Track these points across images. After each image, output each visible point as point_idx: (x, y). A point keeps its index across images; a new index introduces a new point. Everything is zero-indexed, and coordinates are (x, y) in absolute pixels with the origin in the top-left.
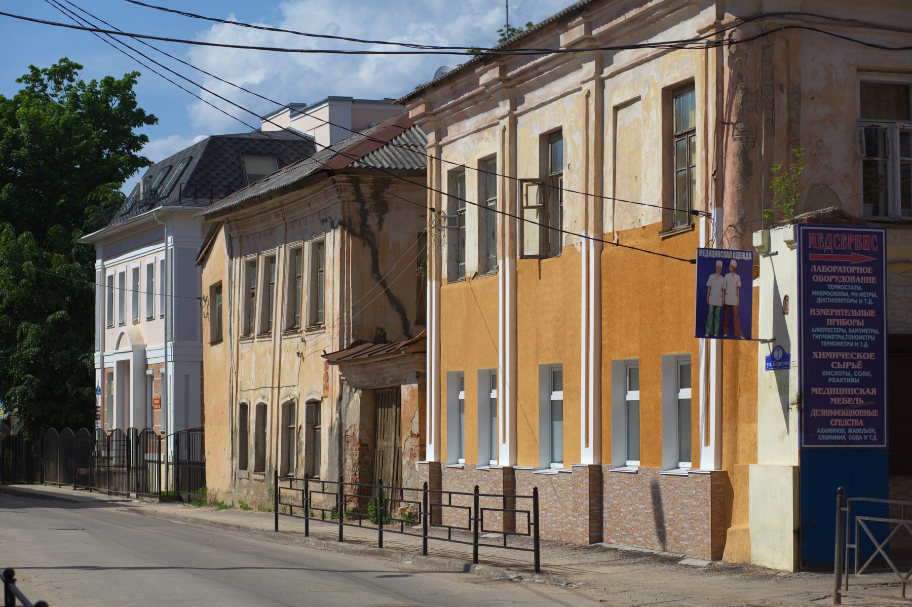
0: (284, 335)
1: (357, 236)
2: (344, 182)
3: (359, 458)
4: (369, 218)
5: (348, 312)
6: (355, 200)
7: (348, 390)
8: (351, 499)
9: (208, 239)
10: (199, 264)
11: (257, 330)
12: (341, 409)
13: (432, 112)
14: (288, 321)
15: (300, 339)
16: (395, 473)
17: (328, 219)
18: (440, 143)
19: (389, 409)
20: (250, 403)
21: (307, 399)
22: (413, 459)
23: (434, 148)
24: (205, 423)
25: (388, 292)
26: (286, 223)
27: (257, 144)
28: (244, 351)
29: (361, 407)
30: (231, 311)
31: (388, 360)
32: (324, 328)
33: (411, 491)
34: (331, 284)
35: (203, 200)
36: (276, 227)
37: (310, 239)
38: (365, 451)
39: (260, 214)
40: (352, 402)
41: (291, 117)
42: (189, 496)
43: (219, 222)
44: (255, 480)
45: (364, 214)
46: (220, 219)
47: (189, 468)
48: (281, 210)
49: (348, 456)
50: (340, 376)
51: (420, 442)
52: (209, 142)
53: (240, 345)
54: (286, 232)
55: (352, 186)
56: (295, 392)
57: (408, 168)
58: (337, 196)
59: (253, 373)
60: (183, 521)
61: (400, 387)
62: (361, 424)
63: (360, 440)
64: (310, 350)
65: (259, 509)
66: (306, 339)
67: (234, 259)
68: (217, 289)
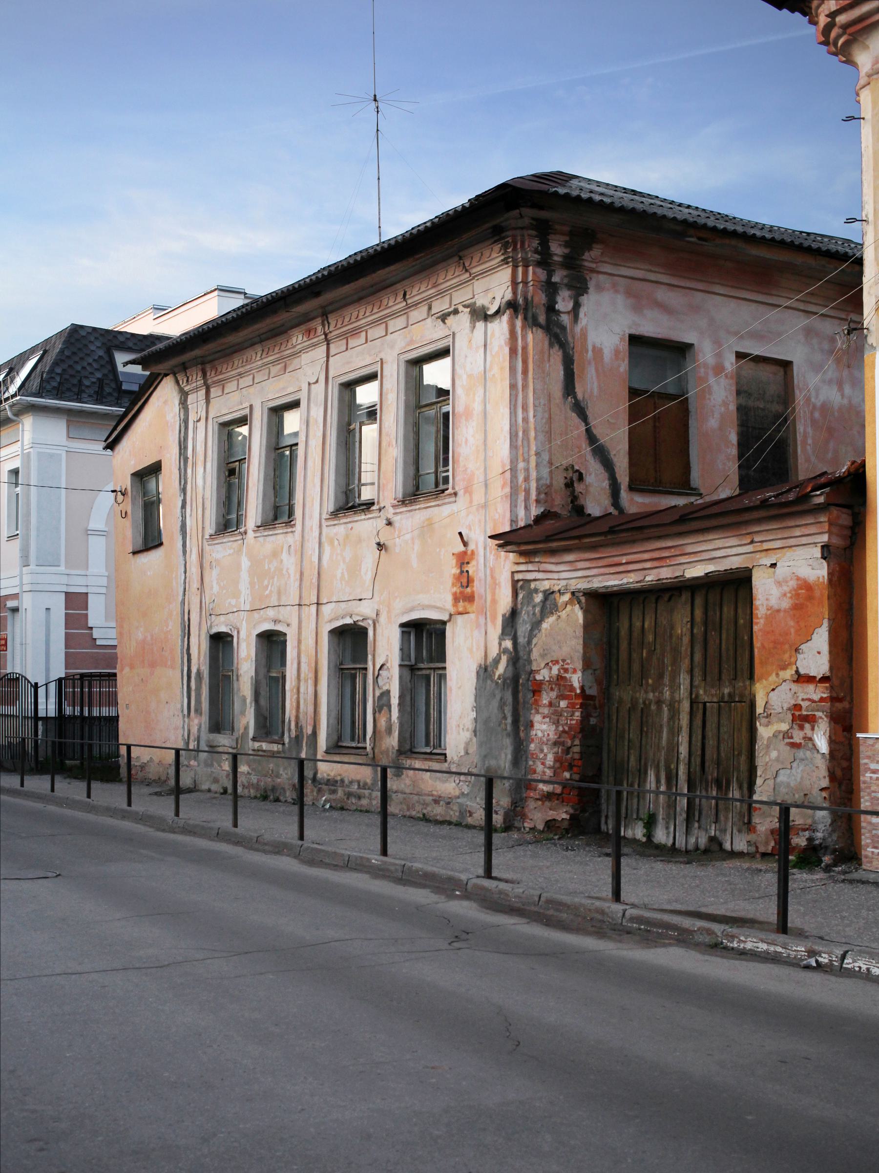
1: (541, 326)
3: (582, 721)
4: (559, 299)
15: (381, 523)
17: (461, 308)
20: (238, 632)
21: (405, 619)
22: (801, 728)
25: (588, 431)
45: (551, 289)
47: (82, 745)
49: (537, 718)
54: (328, 361)
55: (536, 236)
56: (363, 611)
63: (582, 688)
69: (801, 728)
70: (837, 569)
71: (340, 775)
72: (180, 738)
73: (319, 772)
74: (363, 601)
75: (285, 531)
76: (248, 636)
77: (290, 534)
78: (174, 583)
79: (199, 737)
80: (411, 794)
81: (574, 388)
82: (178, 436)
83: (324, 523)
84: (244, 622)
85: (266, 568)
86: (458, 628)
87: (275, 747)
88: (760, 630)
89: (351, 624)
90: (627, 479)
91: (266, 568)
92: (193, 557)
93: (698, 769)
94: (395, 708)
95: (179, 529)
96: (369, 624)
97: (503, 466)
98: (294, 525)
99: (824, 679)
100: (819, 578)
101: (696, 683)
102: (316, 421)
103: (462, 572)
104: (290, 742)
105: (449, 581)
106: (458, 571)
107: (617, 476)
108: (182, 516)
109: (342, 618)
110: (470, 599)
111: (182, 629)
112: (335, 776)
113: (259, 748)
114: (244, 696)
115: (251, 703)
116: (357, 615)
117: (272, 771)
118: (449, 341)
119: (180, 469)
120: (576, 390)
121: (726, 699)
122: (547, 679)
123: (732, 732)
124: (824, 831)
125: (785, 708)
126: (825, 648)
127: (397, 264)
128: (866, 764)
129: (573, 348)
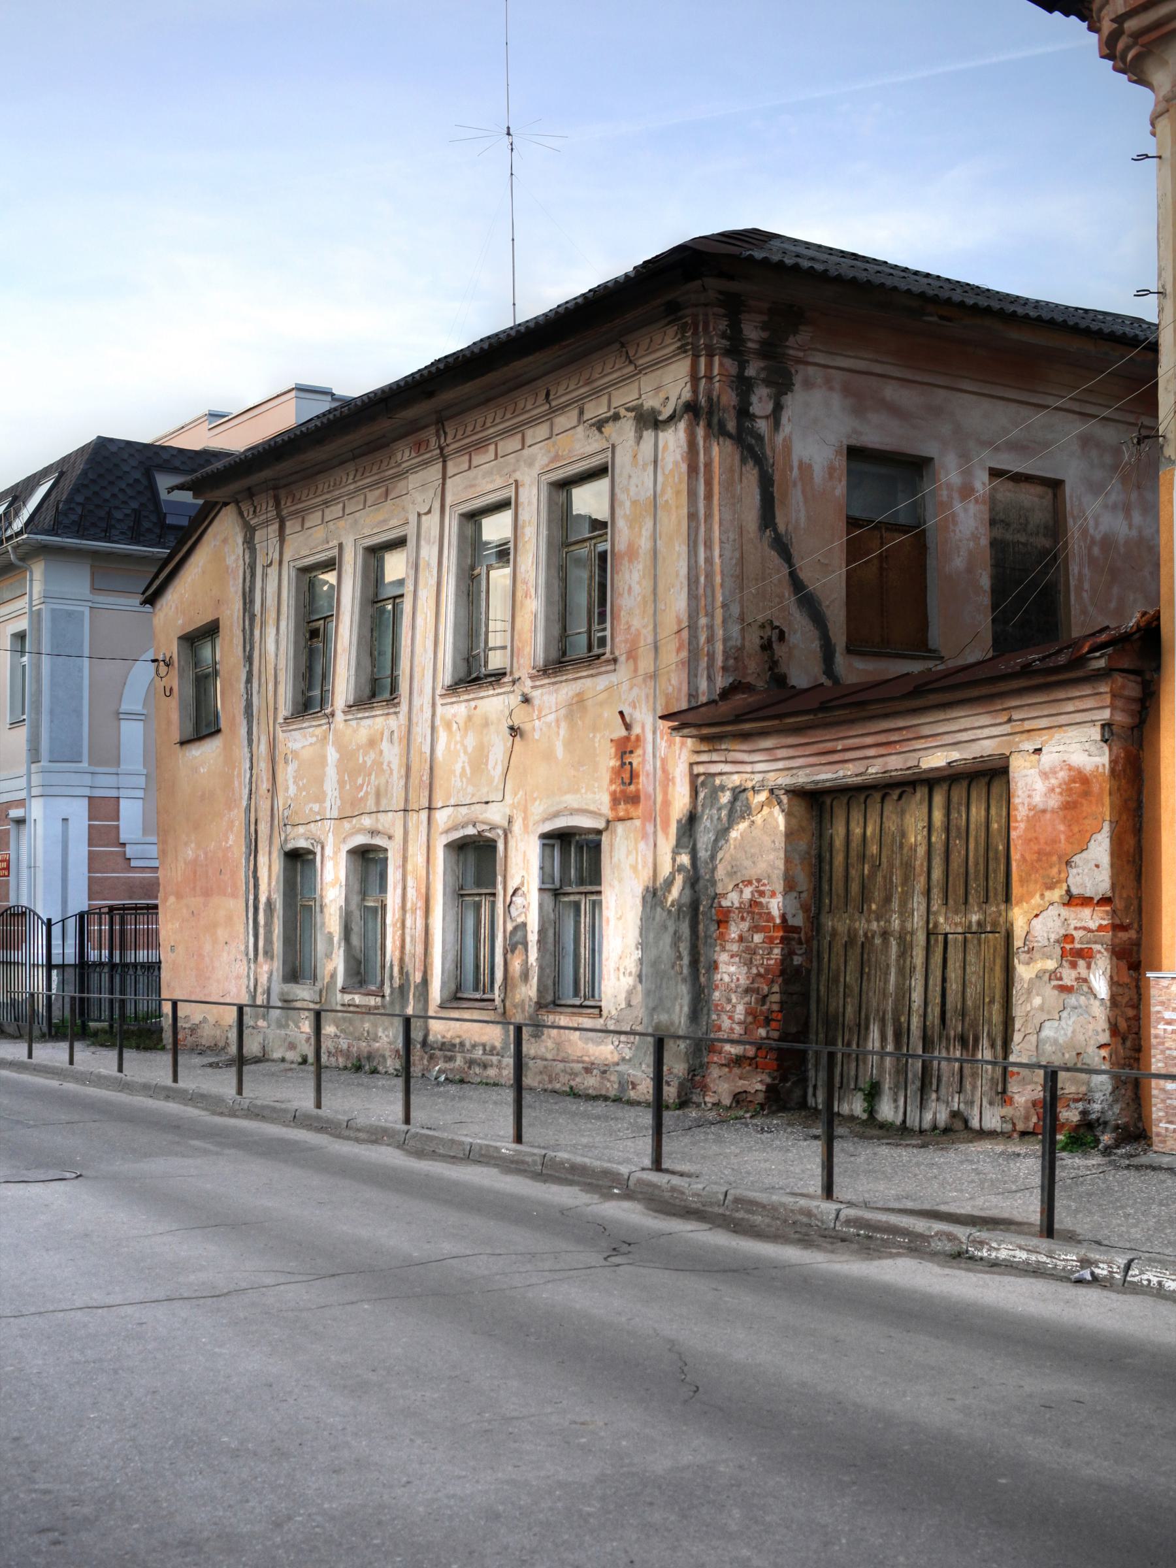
1: (730, 436)
4: (754, 399)
15: (515, 700)
17: (623, 412)
21: (548, 827)
22: (1074, 965)
27: (173, 455)
43: (216, 503)
45: (744, 386)
49: (723, 957)
54: (444, 484)
55: (725, 316)
63: (784, 917)
69: (1074, 965)
70: (1122, 755)
71: (459, 1037)
72: (244, 990)
73: (431, 1033)
74: (490, 804)
77: (393, 717)
79: (269, 989)
80: (554, 1060)
82: (241, 585)
83: (439, 701)
84: (330, 835)
85: (361, 761)
86: (618, 839)
87: (372, 1001)
88: (1019, 837)
90: (844, 638)
96: (498, 834)
98: (399, 703)
99: (1105, 901)
101: (934, 908)
103: (623, 764)
105: (605, 776)
106: (618, 763)
107: (831, 634)
111: (246, 844)
113: (350, 1003)
114: (330, 933)
117: (368, 1032)
121: (974, 928)
123: (981, 973)
124: (1102, 1101)
125: (1052, 940)
126: (1105, 860)
128: (1159, 1012)
129: (773, 465)
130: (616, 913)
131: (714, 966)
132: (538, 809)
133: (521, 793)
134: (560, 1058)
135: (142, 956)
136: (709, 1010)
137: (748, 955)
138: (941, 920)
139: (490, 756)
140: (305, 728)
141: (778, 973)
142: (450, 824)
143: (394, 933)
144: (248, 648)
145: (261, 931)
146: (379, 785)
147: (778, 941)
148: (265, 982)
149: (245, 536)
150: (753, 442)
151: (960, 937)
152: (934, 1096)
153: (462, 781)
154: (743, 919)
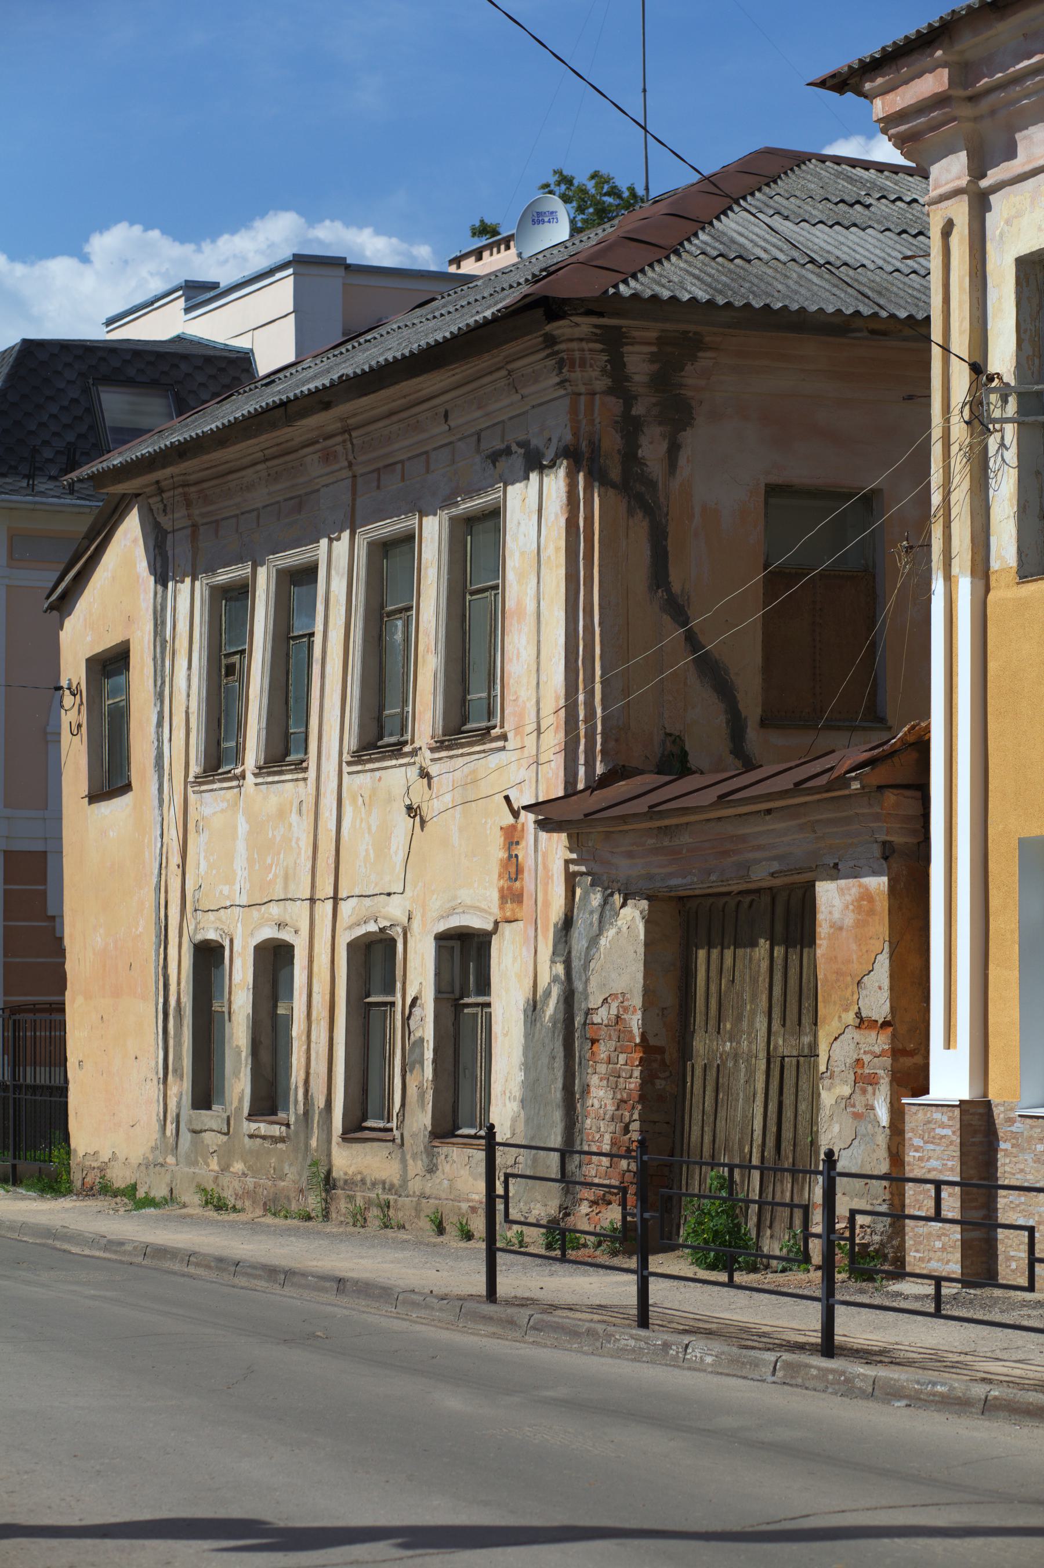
0: (349, 764)
1: (614, 486)
2: (581, 340)
3: (642, 1086)
4: (644, 440)
5: (590, 694)
6: (610, 391)
7: (596, 899)
8: (609, 1197)
9: (86, 542)
10: (52, 608)
11: (253, 753)
12: (569, 952)
13: (970, 92)
14: (361, 726)
15: (413, 772)
16: (773, 1129)
17: (514, 448)
18: (984, 183)
19: (740, 952)
20: (231, 941)
21: (442, 927)
22: (864, 1092)
23: (965, 198)
24: (67, 993)
26: (354, 476)
28: (207, 811)
29: (647, 945)
30: (161, 714)
31: (769, 811)
32: (504, 737)
33: (862, 1182)
34: (531, 619)
35: (8, 480)
36: (318, 490)
37: (442, 508)
38: (655, 1065)
39: (266, 460)
40: (611, 933)
41: (187, 310)
42: (14, 1166)
44: (251, 1136)
46: (120, 488)
47: (15, 1099)
48: (344, 441)
49: (594, 1080)
50: (567, 862)
51: (892, 1042)
52: (20, 351)
53: (192, 797)
54: (354, 500)
55: (602, 351)
56: (394, 910)
57: (757, 306)
58: (557, 380)
59: (240, 863)
60: (105, 1249)
61: (814, 886)
62: (648, 993)
63: (643, 1036)
64: (437, 805)
65: (265, 1210)
66: (433, 770)
67: (170, 584)
68: (104, 667)
69: (864, 1092)
70: (904, 872)
71: (360, 1173)
72: (155, 1118)
73: (334, 1169)
74: (392, 896)
75: (295, 776)
76: (244, 947)
77: (301, 783)
78: (147, 853)
79: (178, 1116)
80: (447, 1199)
81: (667, 575)
82: (152, 601)
83: (346, 769)
84: (239, 925)
85: (270, 835)
86: (505, 942)
87: (276, 1130)
88: (823, 955)
89: (376, 932)
90: (759, 711)
91: (270, 835)
92: (173, 815)
93: (773, 1152)
94: (428, 1066)
95: (153, 761)
96: (398, 933)
97: (557, 698)
98: (307, 768)
99: (886, 1024)
100: (880, 884)
101: (774, 1028)
102: (338, 601)
103: (510, 856)
104: (296, 1119)
105: (495, 869)
106: (506, 855)
107: (741, 706)
108: (158, 740)
109: (365, 922)
110: (517, 898)
111: (156, 932)
112: (354, 1175)
113: (256, 1132)
114: (237, 1046)
115: (246, 1060)
116: (385, 918)
117: (274, 1169)
118: (500, 497)
119: (155, 659)
120: (671, 579)
121: (806, 1051)
122: (605, 1022)
123: (810, 1099)
124: (882, 1233)
125: (847, 1065)
126: (886, 983)
127: (425, 376)
128: (910, 1139)
129: (667, 514)
130: (503, 1028)
131: (586, 1090)
132: (436, 904)
133: (420, 884)
134: (452, 1197)
135: (42, 1077)
136: (582, 1140)
137: (613, 1078)
138: (780, 1042)
139: (393, 838)
140: (216, 790)
141: (637, 1099)
142: (353, 919)
143: (299, 1047)
144: (159, 683)
145: (171, 1042)
146: (287, 867)
147: (637, 1063)
148: (174, 1108)
149: (157, 538)
150: (643, 489)
151: (794, 1060)
152: (768, 1232)
153: (366, 867)
154: (610, 1039)
